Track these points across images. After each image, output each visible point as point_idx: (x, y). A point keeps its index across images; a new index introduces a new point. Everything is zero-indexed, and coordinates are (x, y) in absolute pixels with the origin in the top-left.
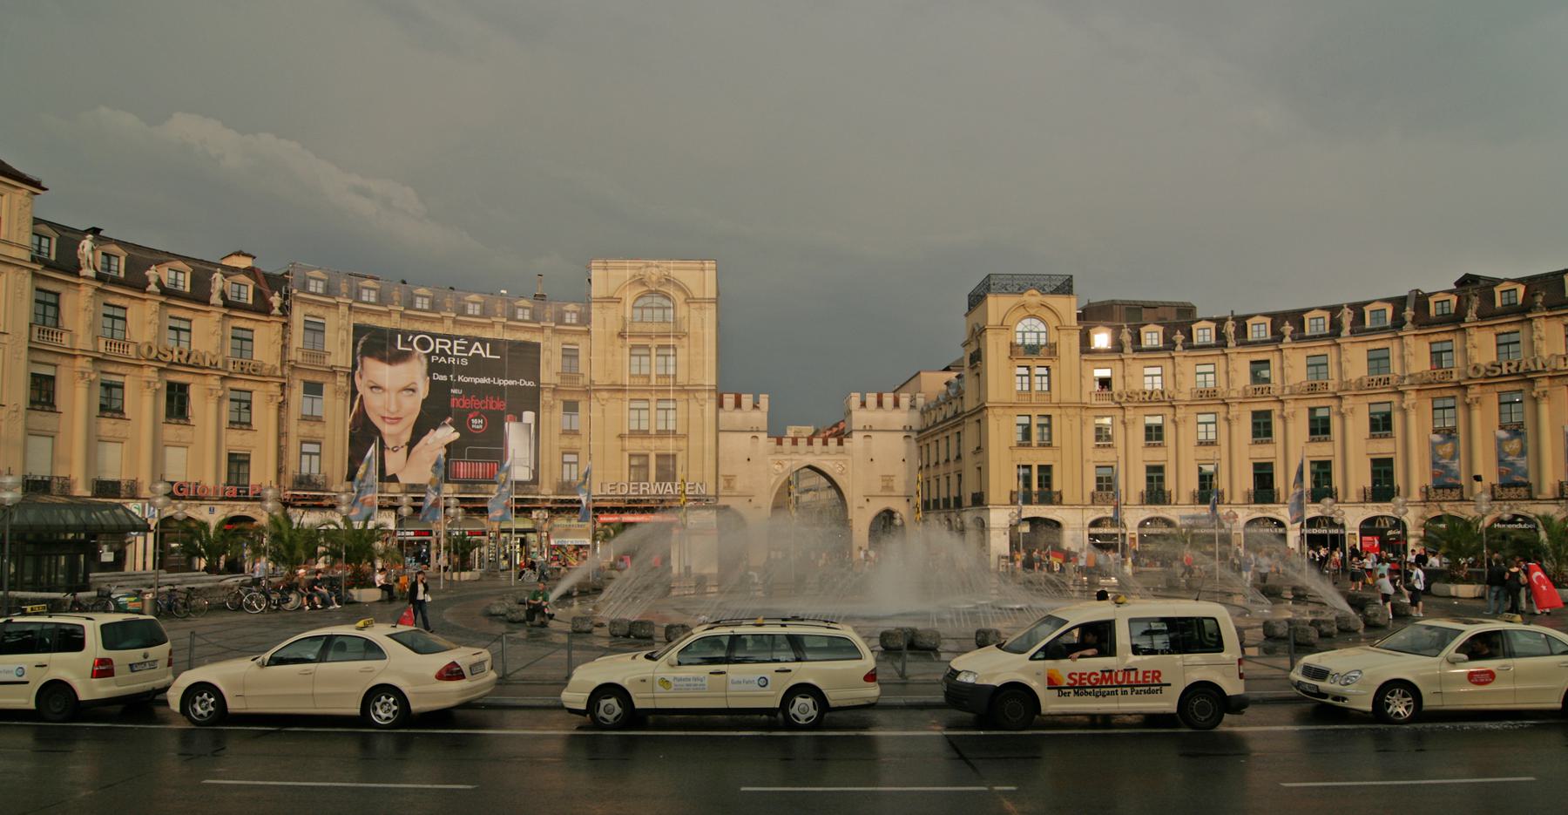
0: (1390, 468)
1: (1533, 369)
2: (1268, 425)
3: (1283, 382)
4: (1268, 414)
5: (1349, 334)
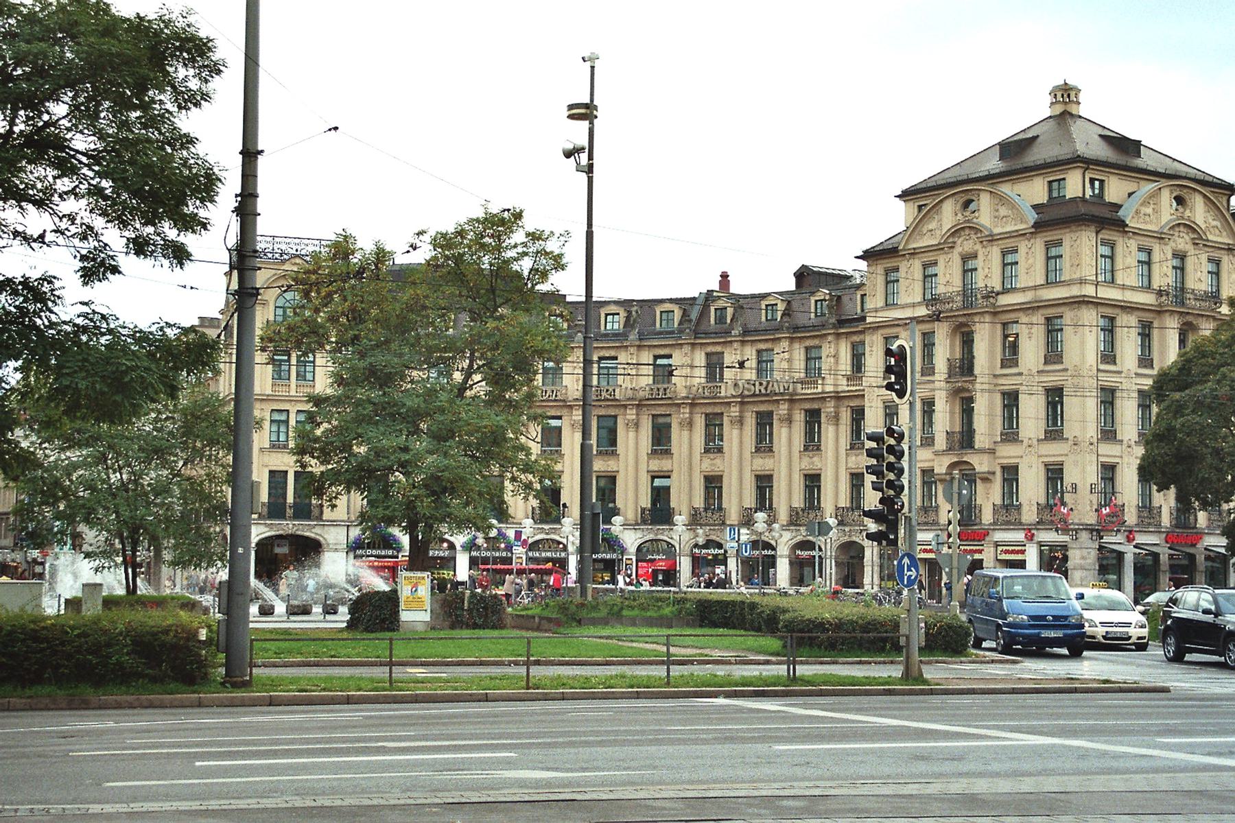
1: (777, 391)
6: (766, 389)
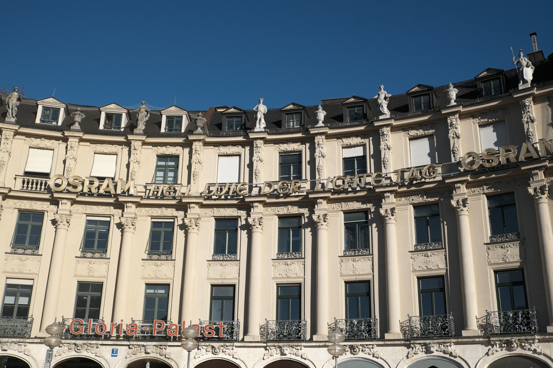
0: (100, 293)
2: (37, 231)
3: (251, 180)
4: (39, 216)
5: (142, 132)
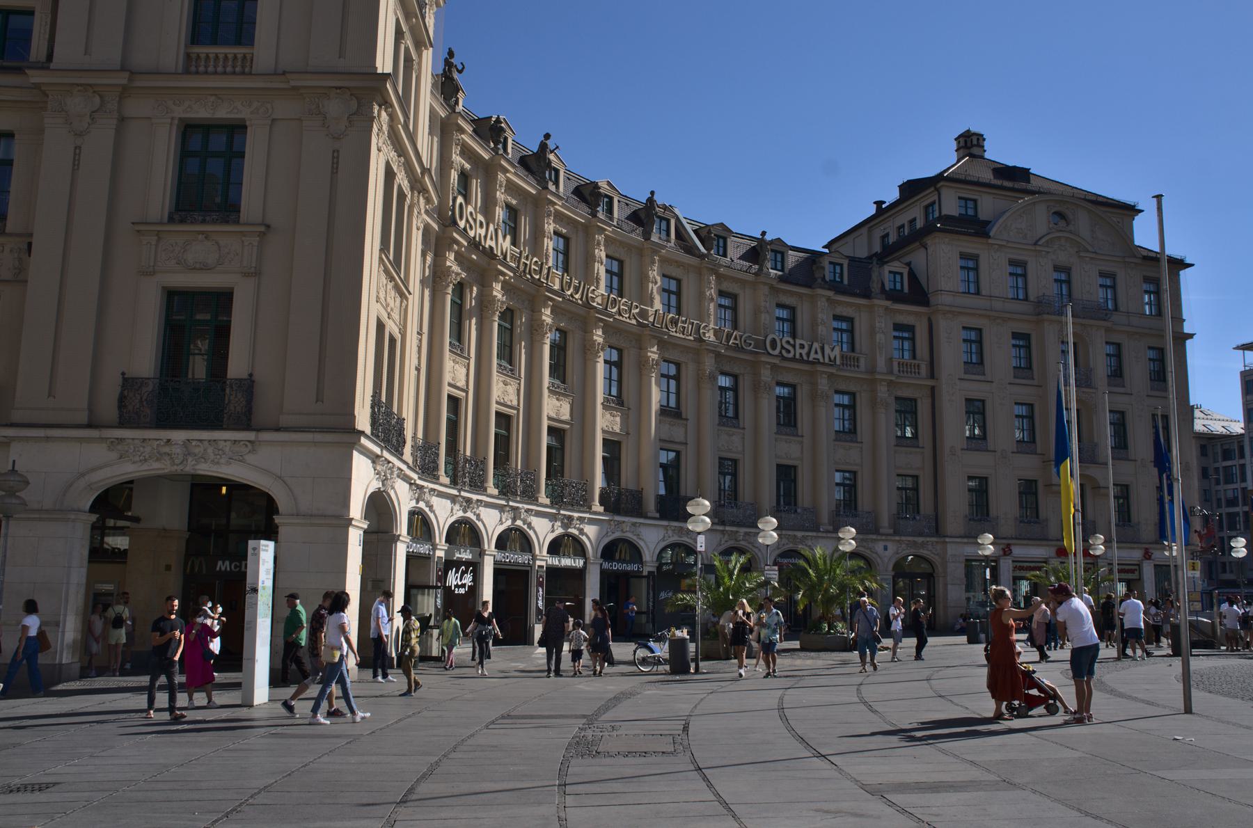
6: (808, 354)
